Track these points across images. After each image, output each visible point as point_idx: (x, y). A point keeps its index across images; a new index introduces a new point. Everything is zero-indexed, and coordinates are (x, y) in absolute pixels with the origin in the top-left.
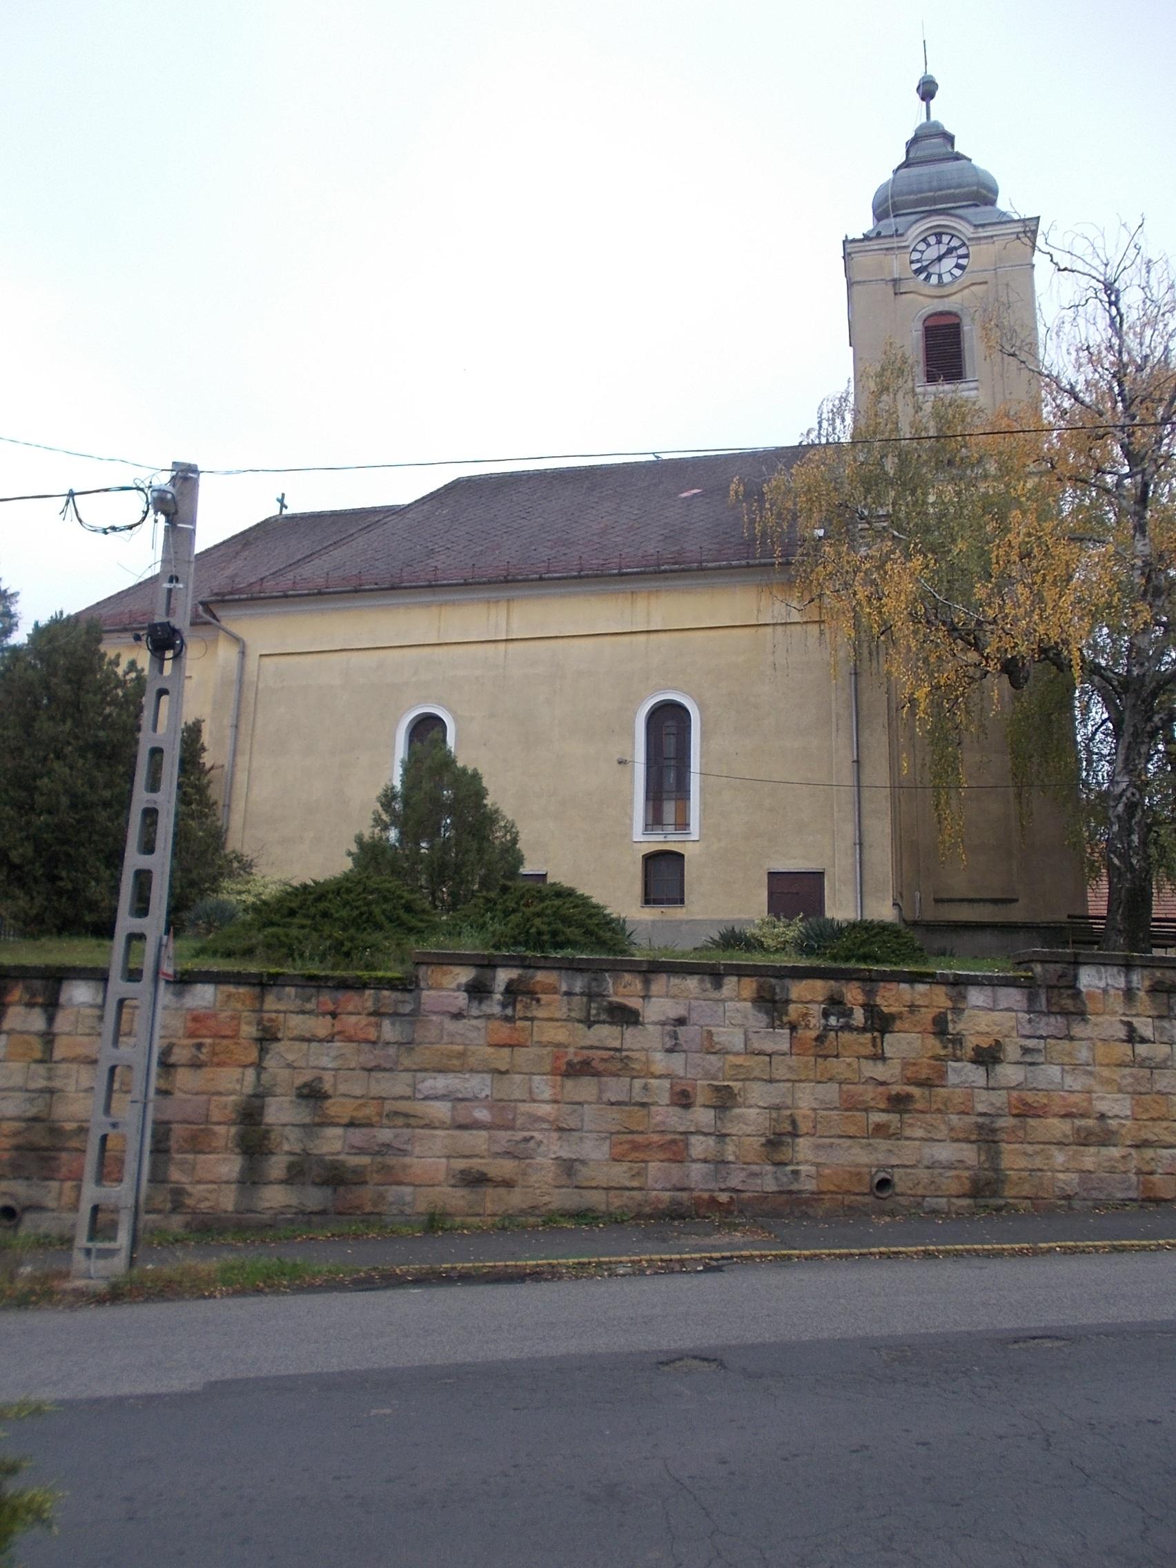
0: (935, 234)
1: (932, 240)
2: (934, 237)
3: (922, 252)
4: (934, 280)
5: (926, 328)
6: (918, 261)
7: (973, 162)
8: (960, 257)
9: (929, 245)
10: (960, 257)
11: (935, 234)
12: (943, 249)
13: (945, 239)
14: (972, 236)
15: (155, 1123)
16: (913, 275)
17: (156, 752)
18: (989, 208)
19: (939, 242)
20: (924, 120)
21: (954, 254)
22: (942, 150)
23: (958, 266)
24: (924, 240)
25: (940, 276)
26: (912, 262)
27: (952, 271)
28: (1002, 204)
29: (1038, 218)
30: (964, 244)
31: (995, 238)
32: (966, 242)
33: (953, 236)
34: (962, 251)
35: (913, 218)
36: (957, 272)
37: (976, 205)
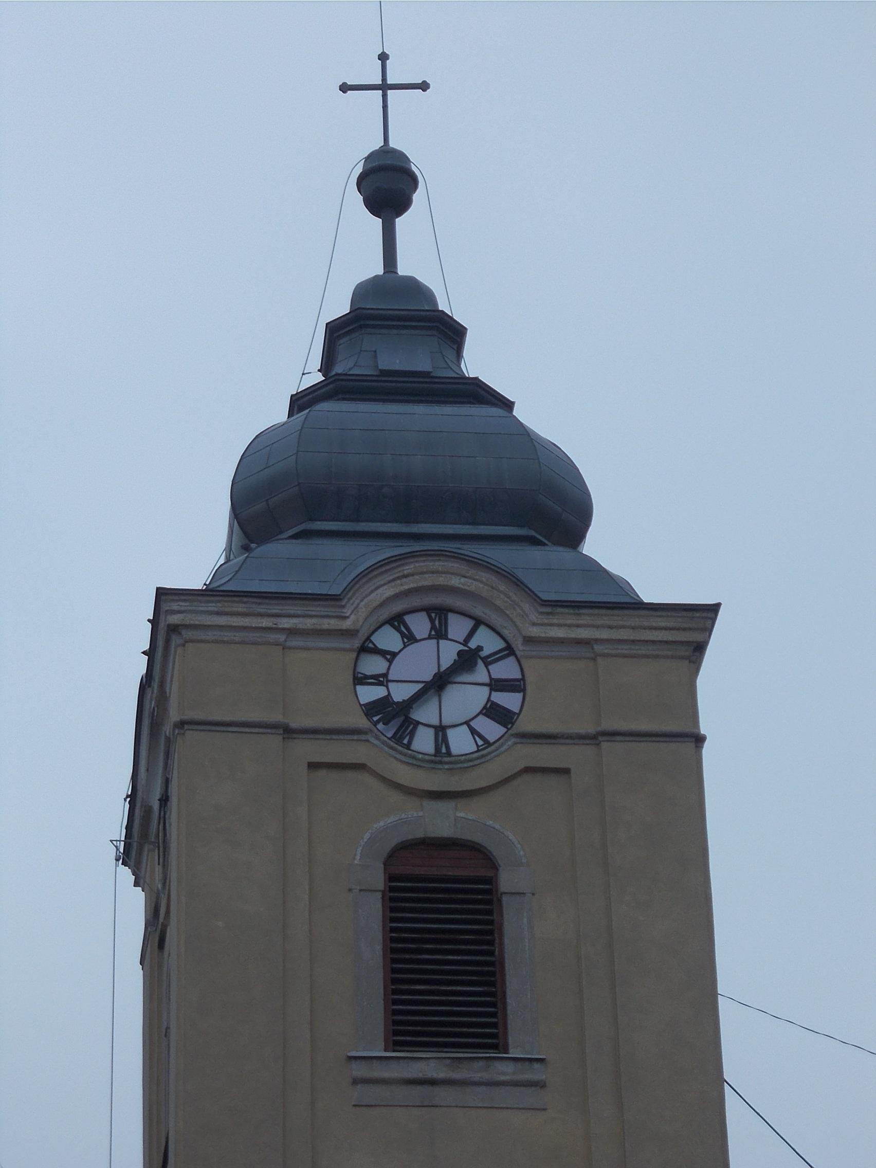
0: (428, 610)
1: (420, 625)
2: (387, 629)
3: (390, 656)
4: (424, 742)
5: (391, 878)
6: (381, 680)
7: (515, 413)
8: (497, 685)
9: (409, 638)
10: (497, 685)
11: (428, 610)
12: (449, 652)
13: (458, 627)
14: (535, 632)
15: (385, 1050)
16: (362, 722)
17: (159, 864)
18: (556, 554)
19: (439, 633)
20: (378, 269)
21: (481, 673)
22: (421, 361)
23: (493, 711)
24: (397, 621)
25: (441, 730)
26: (360, 680)
27: (477, 724)
28: (592, 548)
29: (714, 609)
30: (509, 651)
31: (598, 648)
32: (518, 645)
33: (479, 622)
34: (506, 669)
35: (221, 588)
36: (492, 730)
37: (533, 541)
